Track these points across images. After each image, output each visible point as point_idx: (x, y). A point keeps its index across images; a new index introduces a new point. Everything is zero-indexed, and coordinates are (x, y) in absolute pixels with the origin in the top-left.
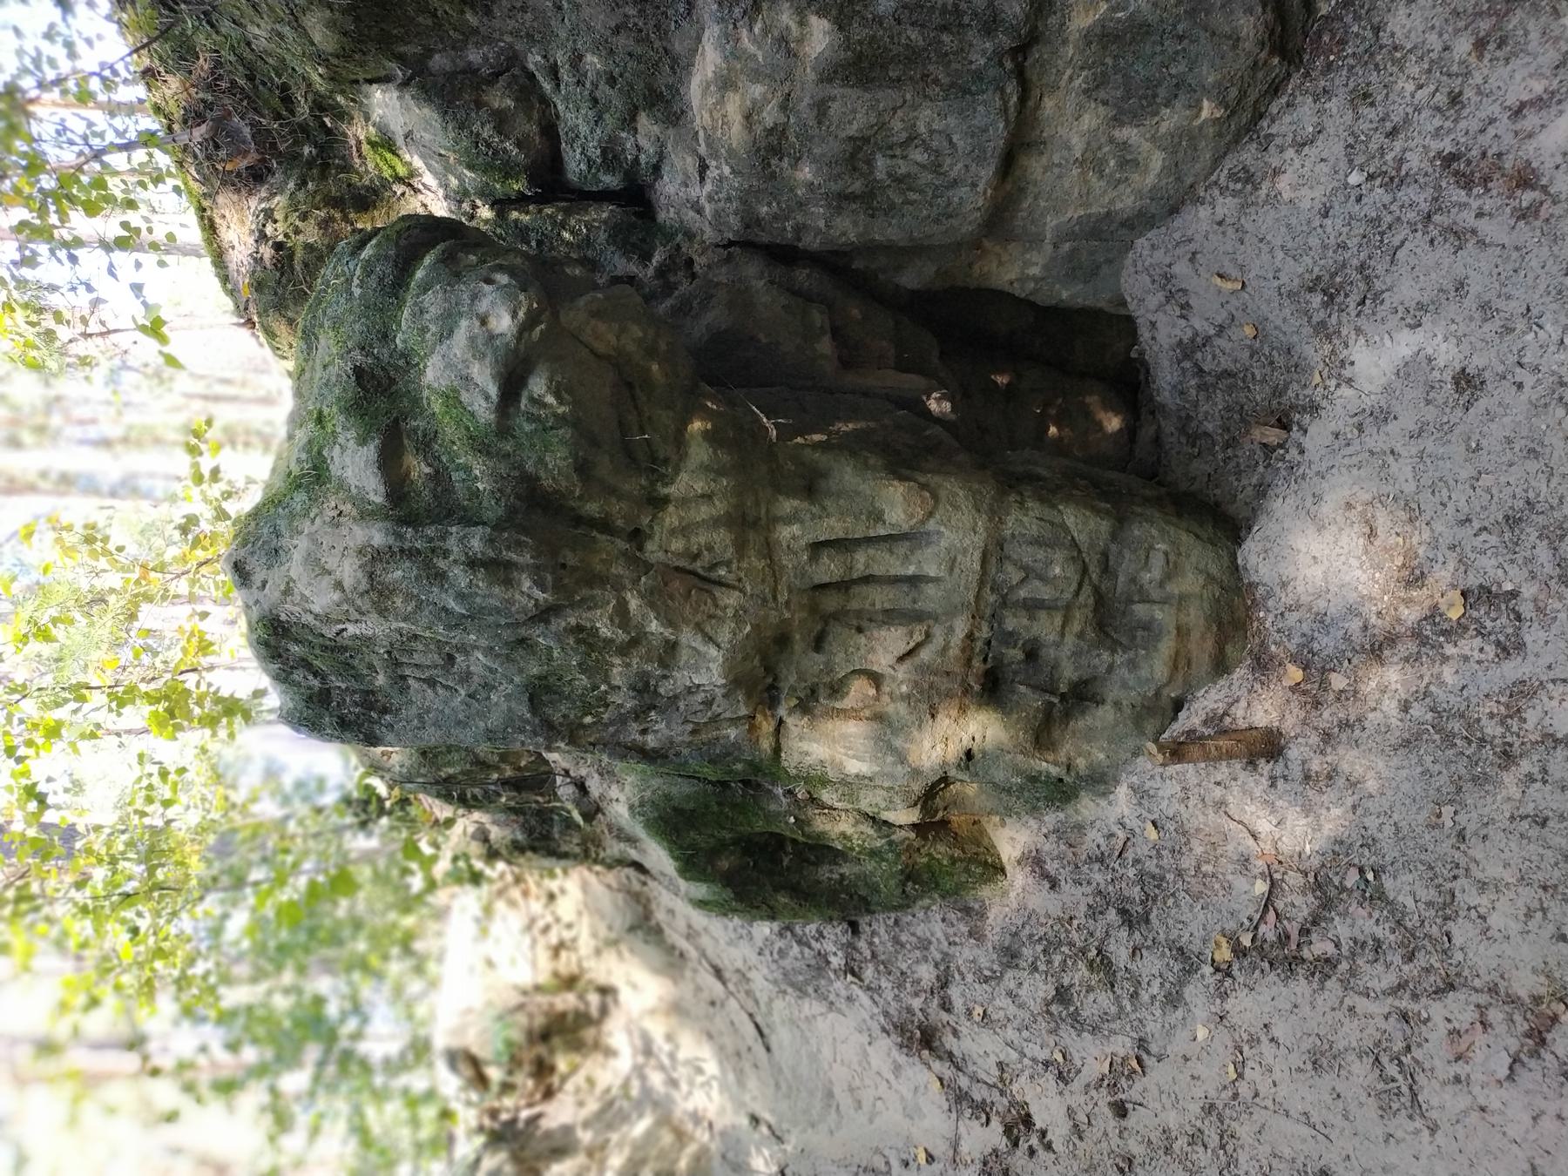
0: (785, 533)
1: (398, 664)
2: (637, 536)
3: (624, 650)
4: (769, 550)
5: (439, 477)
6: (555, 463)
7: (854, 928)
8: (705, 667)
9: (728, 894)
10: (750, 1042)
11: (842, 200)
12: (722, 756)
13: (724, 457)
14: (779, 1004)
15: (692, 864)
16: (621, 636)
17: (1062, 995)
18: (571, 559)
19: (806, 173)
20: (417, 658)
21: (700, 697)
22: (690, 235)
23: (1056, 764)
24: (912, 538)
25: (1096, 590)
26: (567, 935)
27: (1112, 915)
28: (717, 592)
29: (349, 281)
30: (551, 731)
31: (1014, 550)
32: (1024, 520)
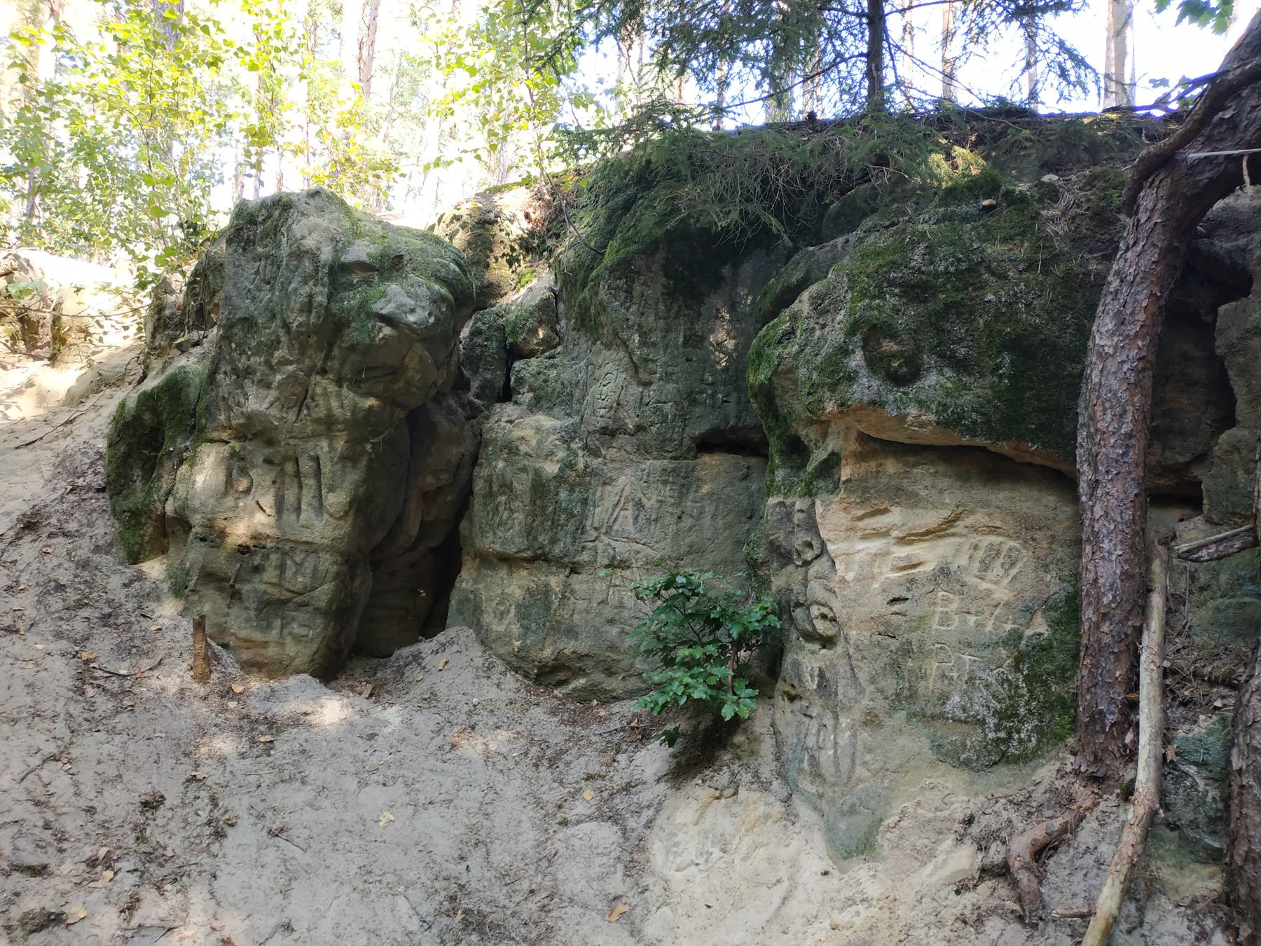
0: (324, 444)
1: (267, 258)
2: (323, 372)
3: (267, 362)
4: (315, 435)
5: (351, 286)
6: (353, 335)
7: (101, 490)
8: (257, 402)
9: (129, 418)
10: (22, 438)
11: (489, 482)
12: (209, 412)
13: (360, 415)
14: (49, 454)
15: (147, 400)
16: (274, 361)
17: (60, 587)
18: (313, 340)
19: (501, 464)
20: (269, 267)
21: (242, 400)
22: (487, 418)
23: (196, 584)
24: (320, 507)
25: (289, 600)
26: (95, 338)
27: (107, 610)
28: (296, 409)
29: (441, 257)
30: (229, 327)
31: (312, 558)
32: (327, 563)
